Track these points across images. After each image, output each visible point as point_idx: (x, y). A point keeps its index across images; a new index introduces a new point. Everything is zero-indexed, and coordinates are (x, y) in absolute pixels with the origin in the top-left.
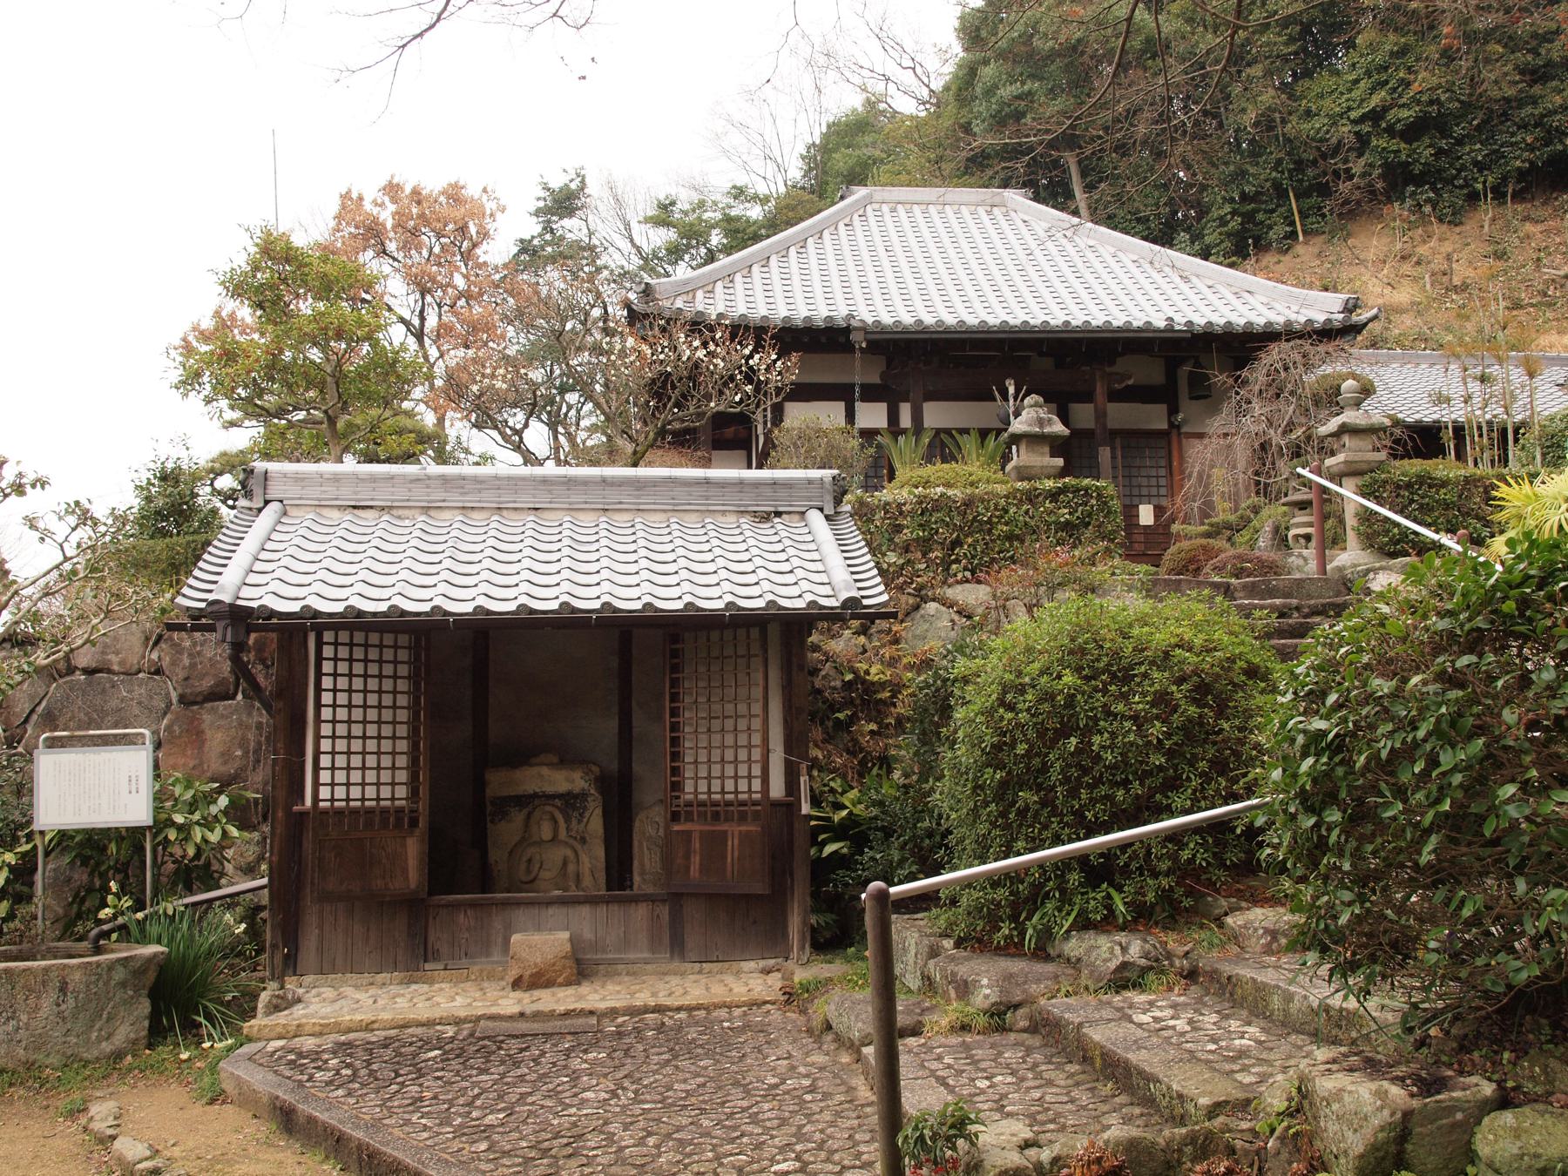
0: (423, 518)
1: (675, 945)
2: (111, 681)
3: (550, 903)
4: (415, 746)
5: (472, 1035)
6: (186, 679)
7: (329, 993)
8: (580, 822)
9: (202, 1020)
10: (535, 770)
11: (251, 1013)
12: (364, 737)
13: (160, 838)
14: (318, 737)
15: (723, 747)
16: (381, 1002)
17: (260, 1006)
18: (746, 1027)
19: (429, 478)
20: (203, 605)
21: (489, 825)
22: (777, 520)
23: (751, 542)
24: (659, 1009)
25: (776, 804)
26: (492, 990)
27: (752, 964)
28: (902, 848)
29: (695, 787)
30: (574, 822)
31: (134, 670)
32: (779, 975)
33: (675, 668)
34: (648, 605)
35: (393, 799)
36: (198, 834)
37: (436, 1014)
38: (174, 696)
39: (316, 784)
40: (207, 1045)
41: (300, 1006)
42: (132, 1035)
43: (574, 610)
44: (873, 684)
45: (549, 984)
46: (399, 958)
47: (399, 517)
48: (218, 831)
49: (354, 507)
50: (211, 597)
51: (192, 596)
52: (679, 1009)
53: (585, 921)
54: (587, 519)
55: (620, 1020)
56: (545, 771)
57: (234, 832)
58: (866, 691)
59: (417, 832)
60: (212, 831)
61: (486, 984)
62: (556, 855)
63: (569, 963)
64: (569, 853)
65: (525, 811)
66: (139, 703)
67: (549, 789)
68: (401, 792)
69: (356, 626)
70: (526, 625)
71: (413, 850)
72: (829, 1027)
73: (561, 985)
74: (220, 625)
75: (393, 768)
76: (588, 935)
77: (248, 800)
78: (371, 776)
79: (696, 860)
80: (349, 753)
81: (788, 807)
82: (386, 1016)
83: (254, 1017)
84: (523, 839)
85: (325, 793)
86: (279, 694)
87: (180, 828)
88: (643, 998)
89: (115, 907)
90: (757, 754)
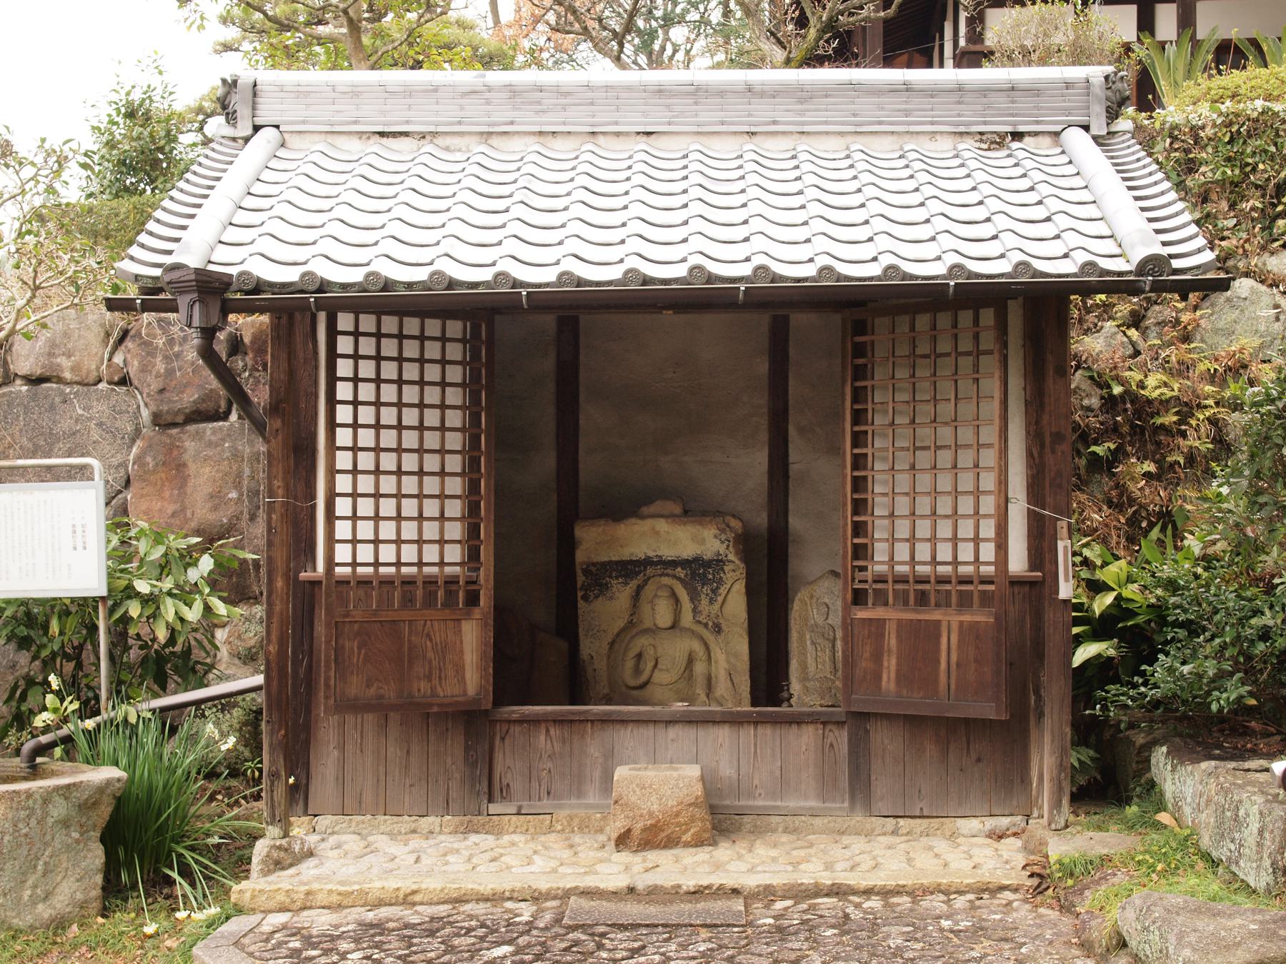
0: (483, 148)
1: (858, 786)
2: (62, 393)
3: (670, 722)
4: (473, 487)
5: (558, 921)
6: (162, 391)
7: (352, 842)
8: (712, 601)
9: (175, 875)
10: (649, 523)
11: (241, 867)
12: (399, 473)
13: (117, 616)
14: (332, 472)
15: (935, 493)
16: (426, 861)
17: (255, 860)
18: (979, 931)
19: (490, 89)
20: (157, 272)
21: (581, 603)
22: (1015, 145)
23: (980, 176)
24: (837, 891)
25: (1016, 582)
26: (588, 848)
27: (973, 824)
28: (1219, 654)
29: (890, 553)
30: (704, 601)
31: (91, 379)
32: (1016, 843)
33: (860, 373)
34: (826, 269)
35: (442, 564)
36: (169, 609)
37: (505, 883)
38: (145, 413)
39: (331, 540)
40: (181, 915)
41: (311, 862)
42: (79, 896)
43: (711, 278)
44: (1149, 402)
45: (671, 843)
46: (454, 794)
47: (447, 149)
48: (198, 606)
49: (382, 134)
50: (168, 260)
51: (141, 261)
52: (868, 892)
53: (725, 751)
54: (724, 147)
55: (780, 905)
56: (662, 525)
57: (220, 608)
58: (1138, 413)
59: (477, 613)
60: (189, 605)
61: (577, 839)
62: (675, 650)
63: (701, 813)
64: (697, 646)
65: (634, 584)
66: (100, 425)
67: (668, 553)
68: (454, 554)
69: (390, 306)
70: (640, 303)
71: (472, 639)
72: (1123, 944)
73: (687, 845)
74: (183, 301)
75: (442, 518)
76: (727, 770)
77: (245, 561)
78: (409, 531)
79: (891, 664)
80: (377, 496)
81: (1036, 588)
82: (433, 884)
83: (247, 878)
84: (631, 624)
85: (343, 553)
86: (275, 408)
87: (147, 600)
88: (812, 873)
89: (55, 710)
90: (988, 504)
